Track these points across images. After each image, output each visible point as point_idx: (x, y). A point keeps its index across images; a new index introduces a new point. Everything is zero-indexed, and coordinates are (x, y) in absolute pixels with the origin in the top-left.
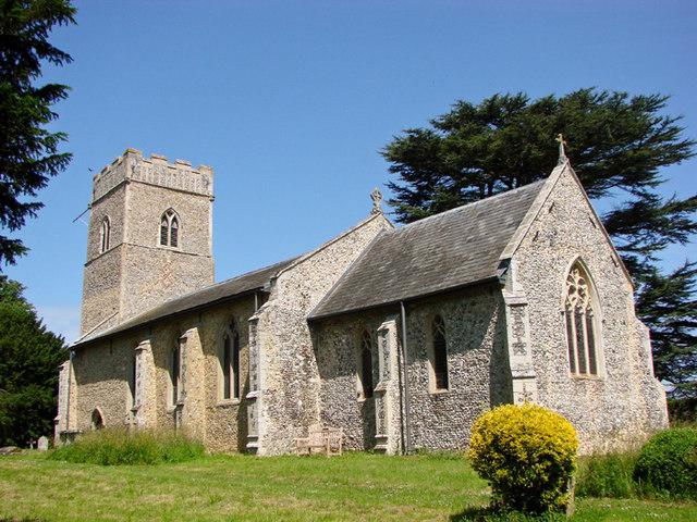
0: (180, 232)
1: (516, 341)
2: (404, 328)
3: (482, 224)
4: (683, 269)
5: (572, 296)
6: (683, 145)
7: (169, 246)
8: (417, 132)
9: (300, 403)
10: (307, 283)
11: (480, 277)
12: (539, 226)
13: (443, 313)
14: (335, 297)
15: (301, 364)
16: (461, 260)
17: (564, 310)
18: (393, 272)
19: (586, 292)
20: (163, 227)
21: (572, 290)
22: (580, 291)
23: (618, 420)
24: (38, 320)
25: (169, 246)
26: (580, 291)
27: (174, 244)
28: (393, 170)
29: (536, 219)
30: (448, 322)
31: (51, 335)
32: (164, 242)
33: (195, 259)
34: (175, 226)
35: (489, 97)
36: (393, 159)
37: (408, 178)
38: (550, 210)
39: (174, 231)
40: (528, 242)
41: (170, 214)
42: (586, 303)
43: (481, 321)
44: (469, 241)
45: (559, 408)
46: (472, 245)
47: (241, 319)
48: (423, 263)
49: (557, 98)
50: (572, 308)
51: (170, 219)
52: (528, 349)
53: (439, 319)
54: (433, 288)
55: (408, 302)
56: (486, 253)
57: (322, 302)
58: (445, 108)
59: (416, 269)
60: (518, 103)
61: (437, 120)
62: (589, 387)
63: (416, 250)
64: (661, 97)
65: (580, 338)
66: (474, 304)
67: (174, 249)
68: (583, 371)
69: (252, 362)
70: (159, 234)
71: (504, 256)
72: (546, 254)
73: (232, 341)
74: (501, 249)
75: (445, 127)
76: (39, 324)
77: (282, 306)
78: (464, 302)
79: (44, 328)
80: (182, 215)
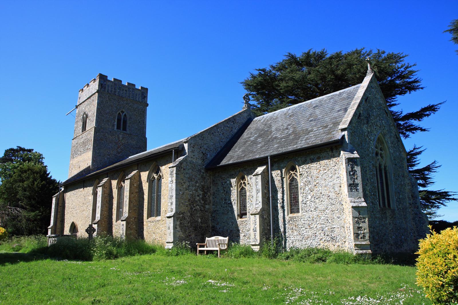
0: (128, 122)
3: (318, 112)
4: (412, 151)
6: (416, 81)
8: (264, 70)
9: (200, 220)
11: (325, 141)
15: (201, 197)
16: (308, 132)
18: (259, 140)
22: (381, 154)
27: (125, 129)
31: (54, 180)
32: (118, 127)
39: (125, 122)
44: (311, 121)
46: (313, 123)
48: (281, 134)
49: (343, 53)
54: (290, 148)
55: (273, 157)
56: (326, 127)
59: (276, 138)
60: (320, 56)
61: (274, 65)
63: (273, 129)
64: (404, 55)
70: (116, 123)
75: (279, 70)
78: (312, 157)
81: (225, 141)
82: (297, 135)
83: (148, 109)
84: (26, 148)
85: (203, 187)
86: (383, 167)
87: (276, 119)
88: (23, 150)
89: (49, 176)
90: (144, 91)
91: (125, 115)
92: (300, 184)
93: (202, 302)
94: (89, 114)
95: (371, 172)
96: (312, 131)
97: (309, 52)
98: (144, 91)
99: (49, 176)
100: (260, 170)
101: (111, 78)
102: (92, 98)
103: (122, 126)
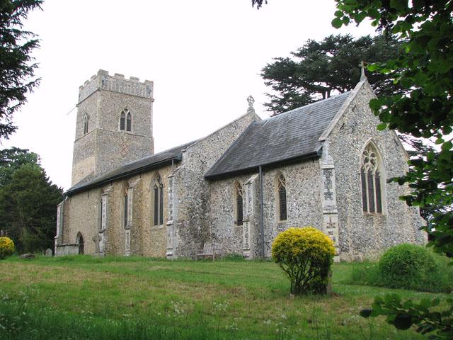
0: (132, 121)
1: (326, 191)
2: (367, 188)
5: (366, 164)
7: (125, 131)
8: (280, 59)
10: (205, 155)
11: (307, 152)
12: (346, 120)
13: (284, 173)
14: (220, 163)
15: (200, 205)
16: (296, 140)
17: (360, 172)
19: (376, 162)
20: (121, 119)
21: (366, 160)
23: (395, 242)
24: (47, 177)
25: (125, 131)
26: (372, 161)
27: (129, 129)
28: (269, 84)
29: (343, 116)
30: (287, 179)
31: (55, 186)
32: (122, 128)
33: (142, 139)
34: (129, 118)
35: (328, 36)
36: (265, 78)
37: (276, 88)
38: (353, 110)
39: (129, 122)
40: (337, 131)
41: (126, 110)
42: (376, 169)
43: (307, 179)
45: (355, 233)
47: (165, 176)
50: (366, 172)
51: (127, 113)
52: (334, 196)
53: (282, 177)
57: (214, 166)
58: (301, 43)
59: (271, 146)
62: (375, 220)
65: (371, 190)
66: (303, 168)
67: (129, 132)
68: (372, 210)
69: (282, 248)
70: (119, 123)
71: (321, 138)
72: (349, 138)
73: (159, 190)
74: (320, 134)
76: (48, 179)
77: (189, 169)
79: (51, 182)
80: (134, 112)
81: (85, 196)
82: (288, 143)
83: (155, 106)
84: (22, 149)
85: (203, 195)
86: (374, 173)
87: (276, 124)
88: (19, 150)
89: (49, 182)
90: (149, 86)
91: (129, 113)
92: (288, 193)
93: (406, 338)
94: (91, 114)
95: (354, 179)
96: (300, 140)
97: (262, 75)
98: (149, 86)
99: (49, 182)
100: (253, 178)
101: (111, 74)
102: (93, 97)
103: (126, 126)
